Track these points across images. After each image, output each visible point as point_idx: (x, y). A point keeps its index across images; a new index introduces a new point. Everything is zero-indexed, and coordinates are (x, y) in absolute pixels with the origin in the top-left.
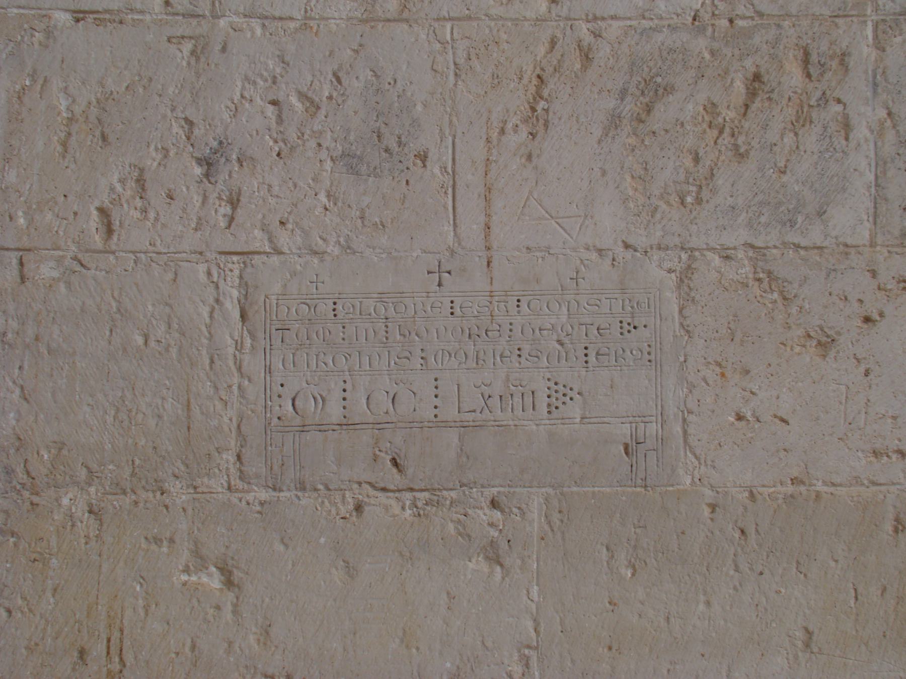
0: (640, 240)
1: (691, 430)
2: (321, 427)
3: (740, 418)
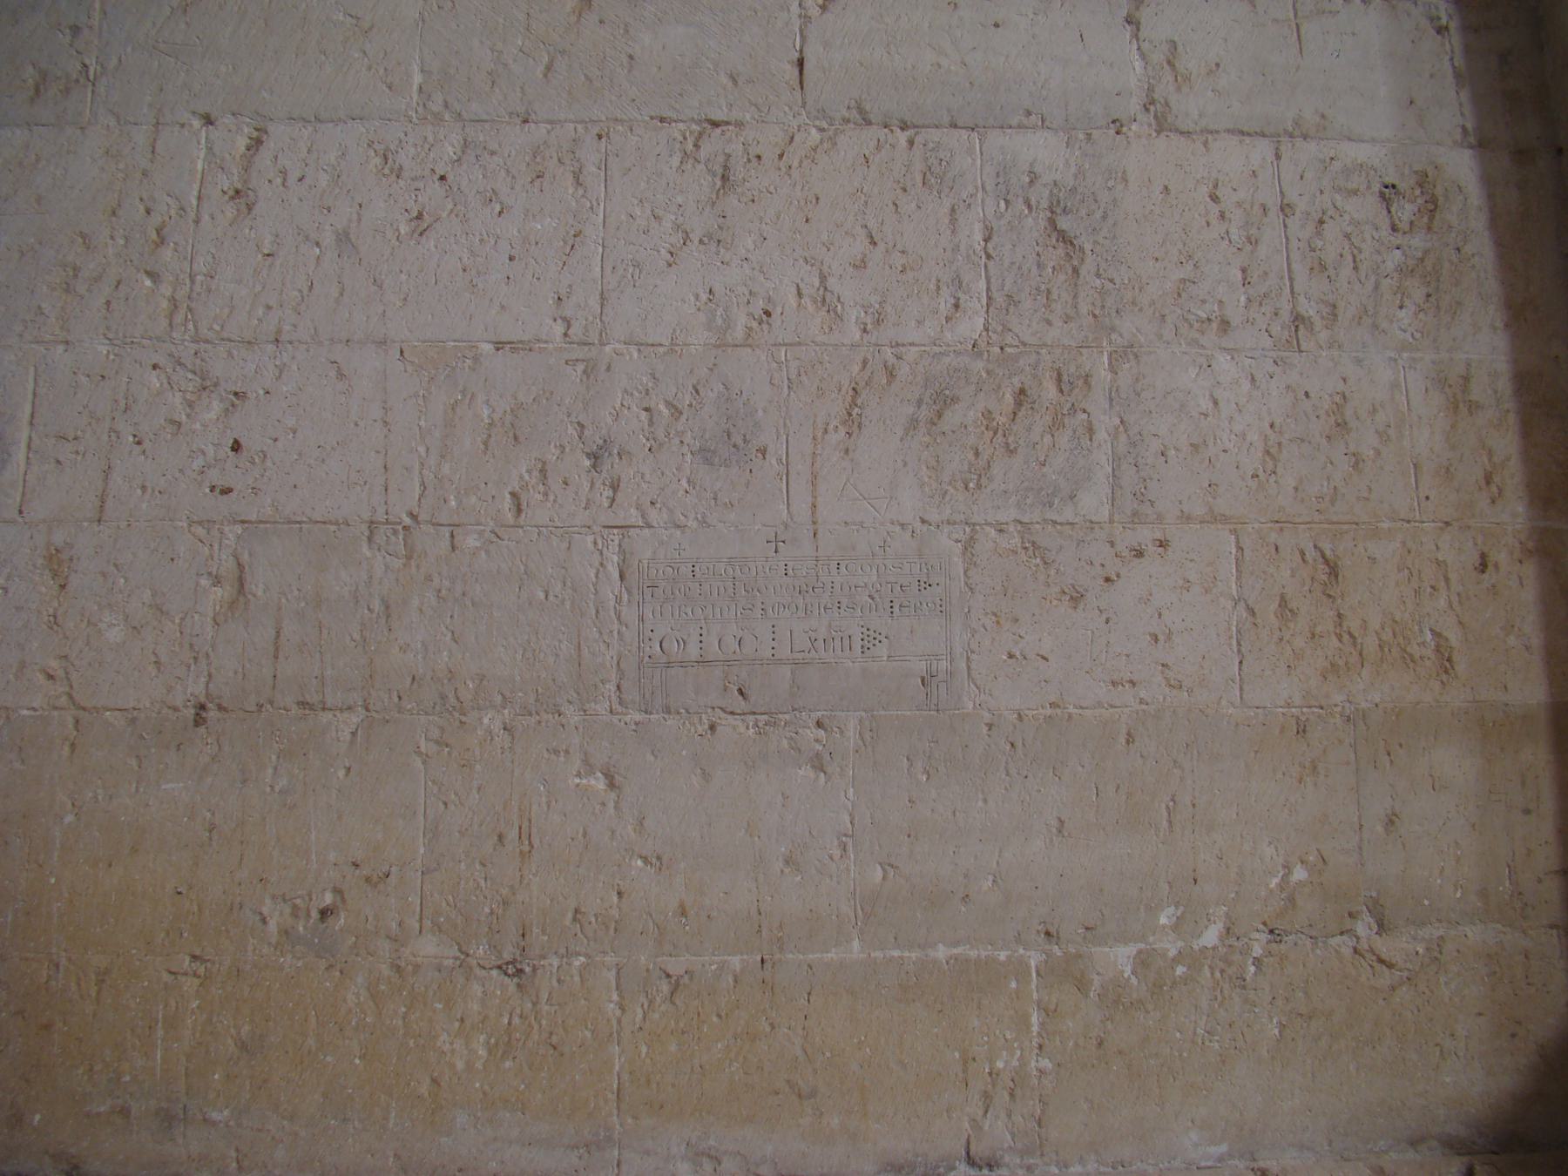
0: (934, 516)
1: (973, 666)
2: (683, 664)
3: (1011, 656)
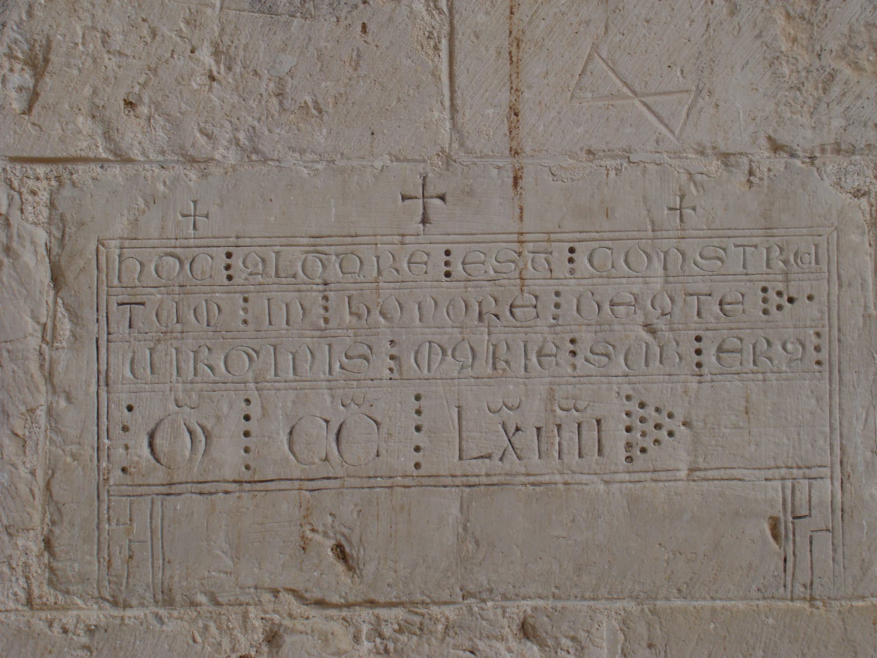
0: (802, 137)
2: (203, 488)
